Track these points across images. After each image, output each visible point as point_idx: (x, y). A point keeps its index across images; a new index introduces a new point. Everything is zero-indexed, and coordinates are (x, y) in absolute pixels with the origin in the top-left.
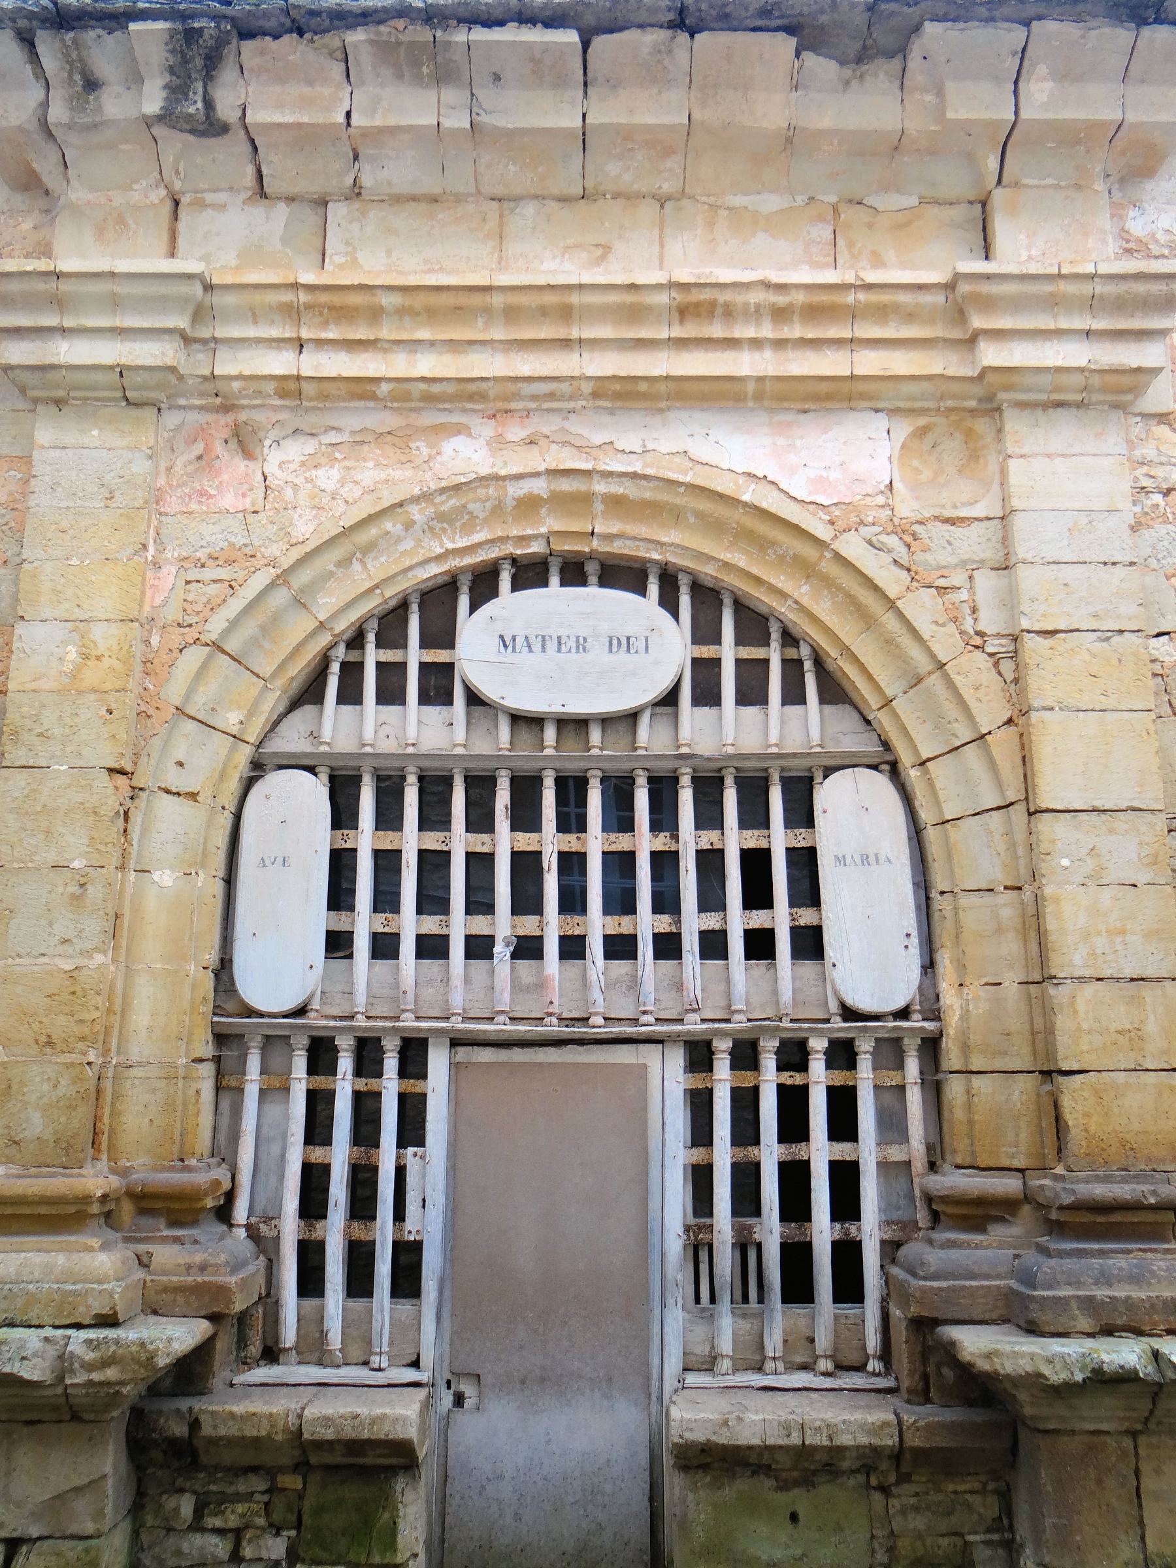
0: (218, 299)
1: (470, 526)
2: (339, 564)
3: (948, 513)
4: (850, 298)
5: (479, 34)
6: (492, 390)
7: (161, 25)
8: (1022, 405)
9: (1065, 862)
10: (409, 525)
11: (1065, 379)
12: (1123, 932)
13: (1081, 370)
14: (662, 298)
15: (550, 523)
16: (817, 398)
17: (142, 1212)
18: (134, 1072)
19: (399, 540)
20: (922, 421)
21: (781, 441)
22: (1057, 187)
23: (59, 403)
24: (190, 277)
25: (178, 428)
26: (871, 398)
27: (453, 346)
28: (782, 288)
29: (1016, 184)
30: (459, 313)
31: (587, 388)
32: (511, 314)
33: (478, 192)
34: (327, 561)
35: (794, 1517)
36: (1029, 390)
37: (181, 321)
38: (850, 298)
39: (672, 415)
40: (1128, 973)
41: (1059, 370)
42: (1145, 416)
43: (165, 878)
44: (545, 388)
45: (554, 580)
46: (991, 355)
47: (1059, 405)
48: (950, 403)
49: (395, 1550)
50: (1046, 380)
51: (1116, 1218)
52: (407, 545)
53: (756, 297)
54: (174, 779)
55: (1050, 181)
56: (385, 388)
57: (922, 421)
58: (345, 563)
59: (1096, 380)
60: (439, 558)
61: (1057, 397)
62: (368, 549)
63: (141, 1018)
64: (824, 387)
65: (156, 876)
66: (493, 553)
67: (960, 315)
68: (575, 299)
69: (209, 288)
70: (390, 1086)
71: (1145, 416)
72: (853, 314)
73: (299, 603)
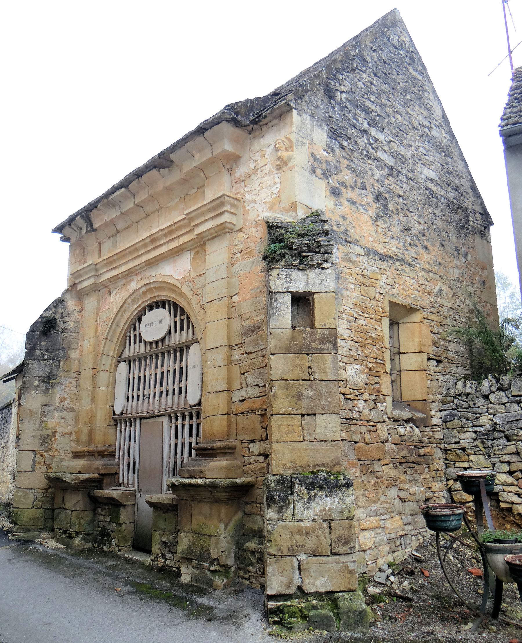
0: (98, 266)
1: (138, 301)
2: (121, 316)
3: (199, 274)
4: (174, 227)
5: (113, 196)
6: (133, 270)
7: (79, 217)
8: (209, 240)
9: (209, 363)
10: (129, 304)
11: (204, 235)
12: (217, 380)
13: (211, 228)
14: (147, 241)
15: (149, 296)
16: (178, 252)
17: (99, 455)
18: (98, 428)
19: (129, 308)
20: (196, 250)
21: (174, 265)
22: (216, 174)
23: (87, 294)
24: (91, 264)
25: (102, 293)
26: (186, 248)
27: (114, 268)
28: (163, 229)
29: (209, 177)
30: (124, 256)
31: (144, 264)
32: (130, 253)
33: (133, 223)
34: (119, 316)
35: (165, 520)
36: (207, 237)
37: (93, 274)
38: (174, 227)
39: (160, 264)
40: (218, 390)
41: (208, 230)
42: (236, 231)
43: (103, 388)
44: (139, 267)
45: (154, 308)
46: (198, 231)
47: (215, 237)
48: (199, 244)
49: (120, 520)
50: (207, 233)
51: (207, 452)
52: (131, 308)
53: (160, 234)
54: (103, 368)
55: (215, 173)
56: (120, 275)
57: (196, 250)
58: (122, 315)
59: (216, 229)
60: (136, 309)
61: (213, 236)
62: (125, 311)
63: (98, 417)
64: (176, 250)
65: (101, 388)
66: (143, 306)
67: (97, 270)
68: (137, 246)
69: (96, 265)
70: (194, 422)
71: (236, 231)
72: (176, 230)
73: (118, 326)
